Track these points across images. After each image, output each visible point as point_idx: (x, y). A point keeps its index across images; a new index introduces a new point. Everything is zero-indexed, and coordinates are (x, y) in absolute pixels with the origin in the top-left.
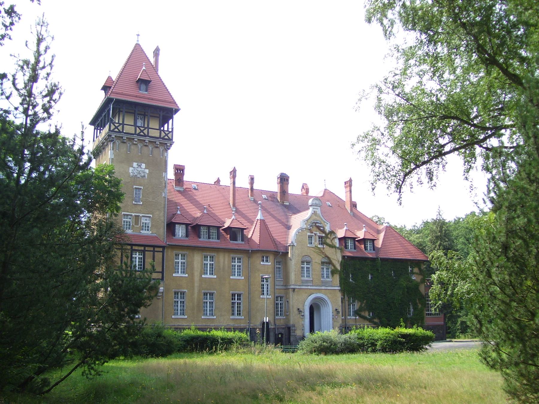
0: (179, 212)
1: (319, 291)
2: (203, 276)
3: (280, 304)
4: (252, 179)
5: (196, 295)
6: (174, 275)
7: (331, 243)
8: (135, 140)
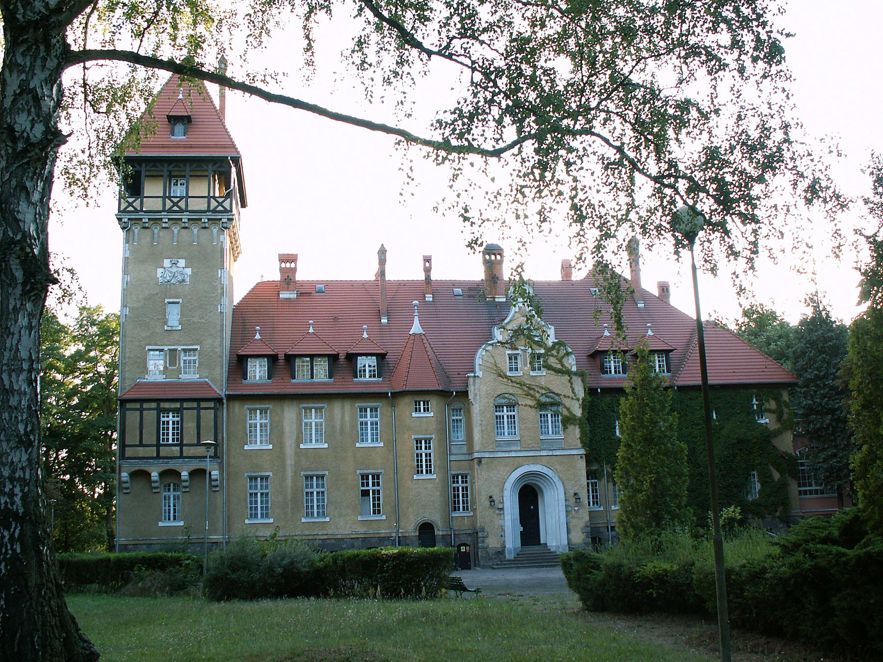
0: (650, 333)
1: (535, 459)
2: (302, 446)
3: (457, 491)
4: (427, 260)
5: (289, 481)
6: (246, 447)
7: (559, 366)
8: (164, 220)
